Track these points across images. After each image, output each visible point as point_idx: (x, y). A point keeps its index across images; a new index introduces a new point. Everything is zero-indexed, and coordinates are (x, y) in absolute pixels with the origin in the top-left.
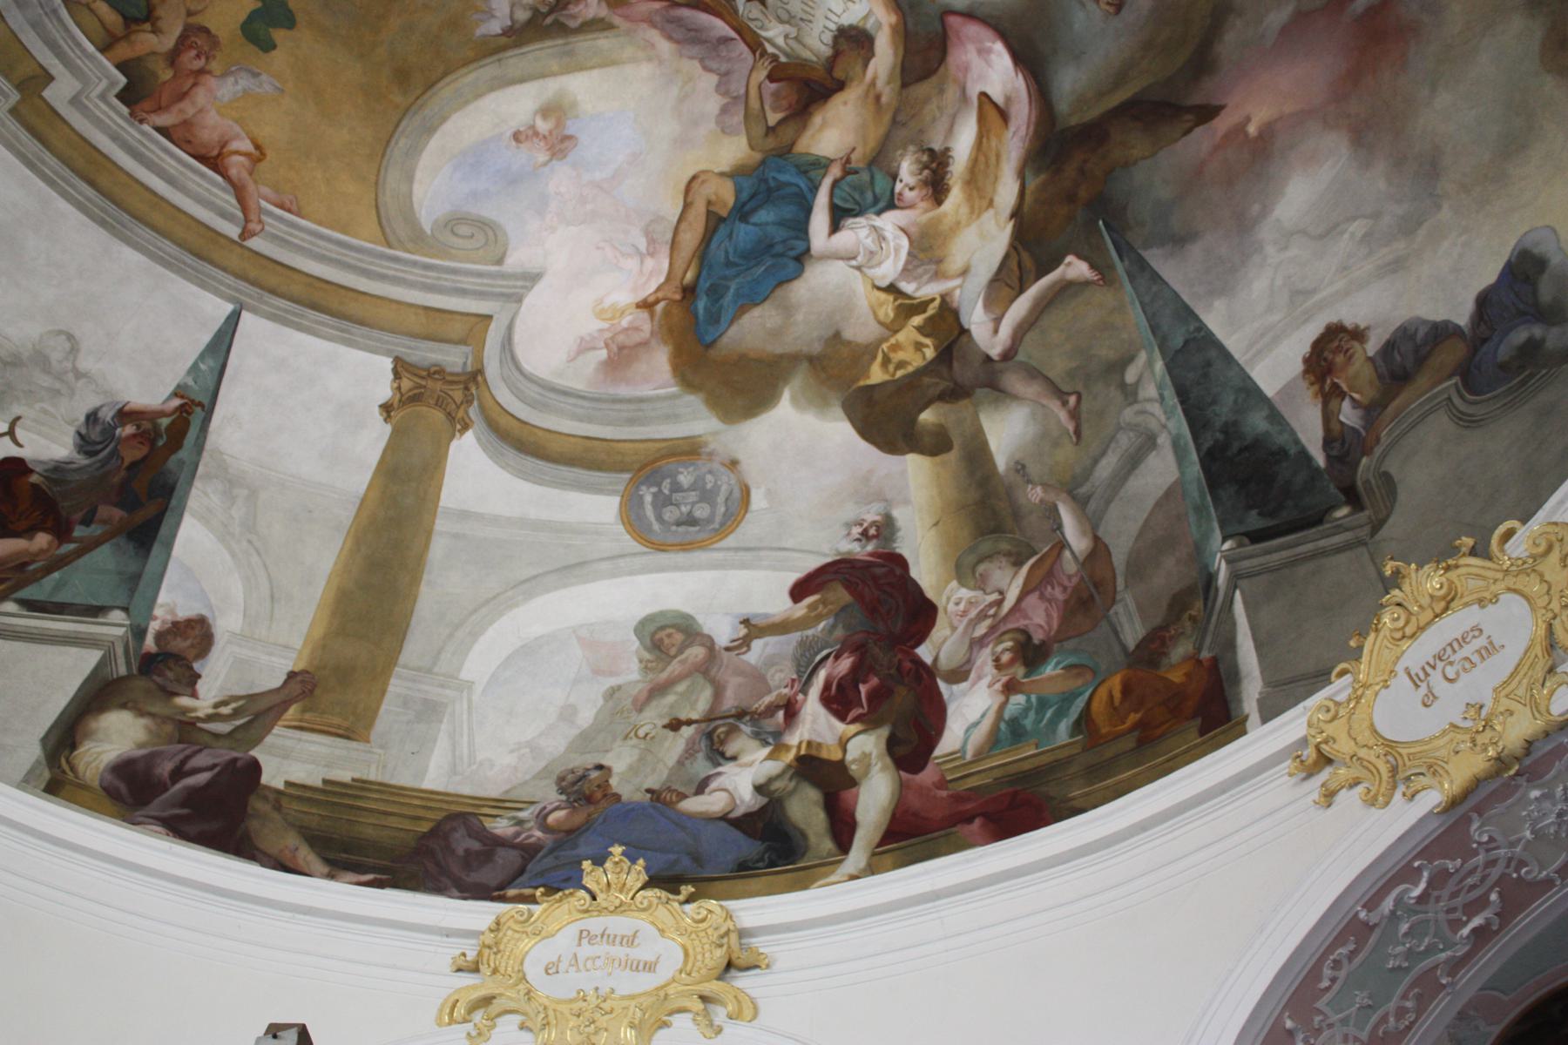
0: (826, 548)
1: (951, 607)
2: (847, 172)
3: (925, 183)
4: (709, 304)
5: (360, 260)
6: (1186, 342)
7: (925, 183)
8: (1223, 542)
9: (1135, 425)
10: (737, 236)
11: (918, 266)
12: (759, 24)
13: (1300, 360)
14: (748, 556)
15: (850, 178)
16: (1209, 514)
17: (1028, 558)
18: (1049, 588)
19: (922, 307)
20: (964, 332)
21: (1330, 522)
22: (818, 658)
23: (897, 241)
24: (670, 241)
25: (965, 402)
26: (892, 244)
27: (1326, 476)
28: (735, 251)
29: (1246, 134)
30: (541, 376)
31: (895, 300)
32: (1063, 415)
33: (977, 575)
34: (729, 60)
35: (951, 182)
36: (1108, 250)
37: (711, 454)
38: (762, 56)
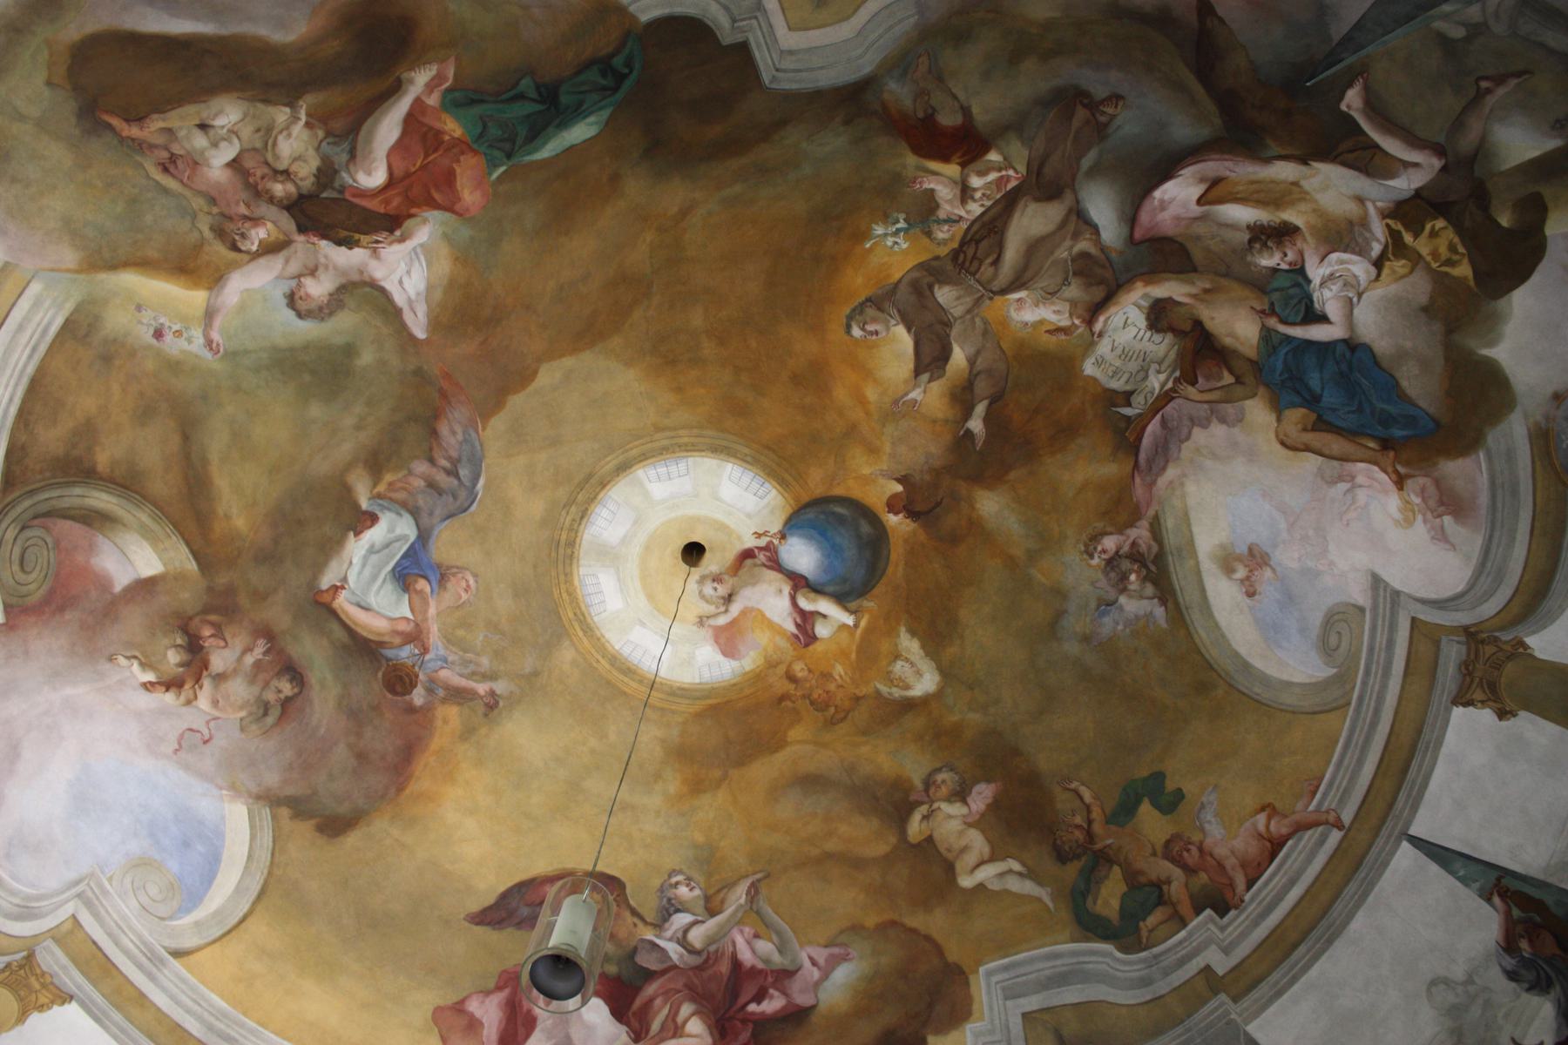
2: (1272, 312)
12: (1149, 395)
19: (1395, 236)
23: (1333, 262)
26: (1336, 268)
31: (1389, 260)
35: (1278, 221)
37: (1547, 418)
38: (1176, 391)
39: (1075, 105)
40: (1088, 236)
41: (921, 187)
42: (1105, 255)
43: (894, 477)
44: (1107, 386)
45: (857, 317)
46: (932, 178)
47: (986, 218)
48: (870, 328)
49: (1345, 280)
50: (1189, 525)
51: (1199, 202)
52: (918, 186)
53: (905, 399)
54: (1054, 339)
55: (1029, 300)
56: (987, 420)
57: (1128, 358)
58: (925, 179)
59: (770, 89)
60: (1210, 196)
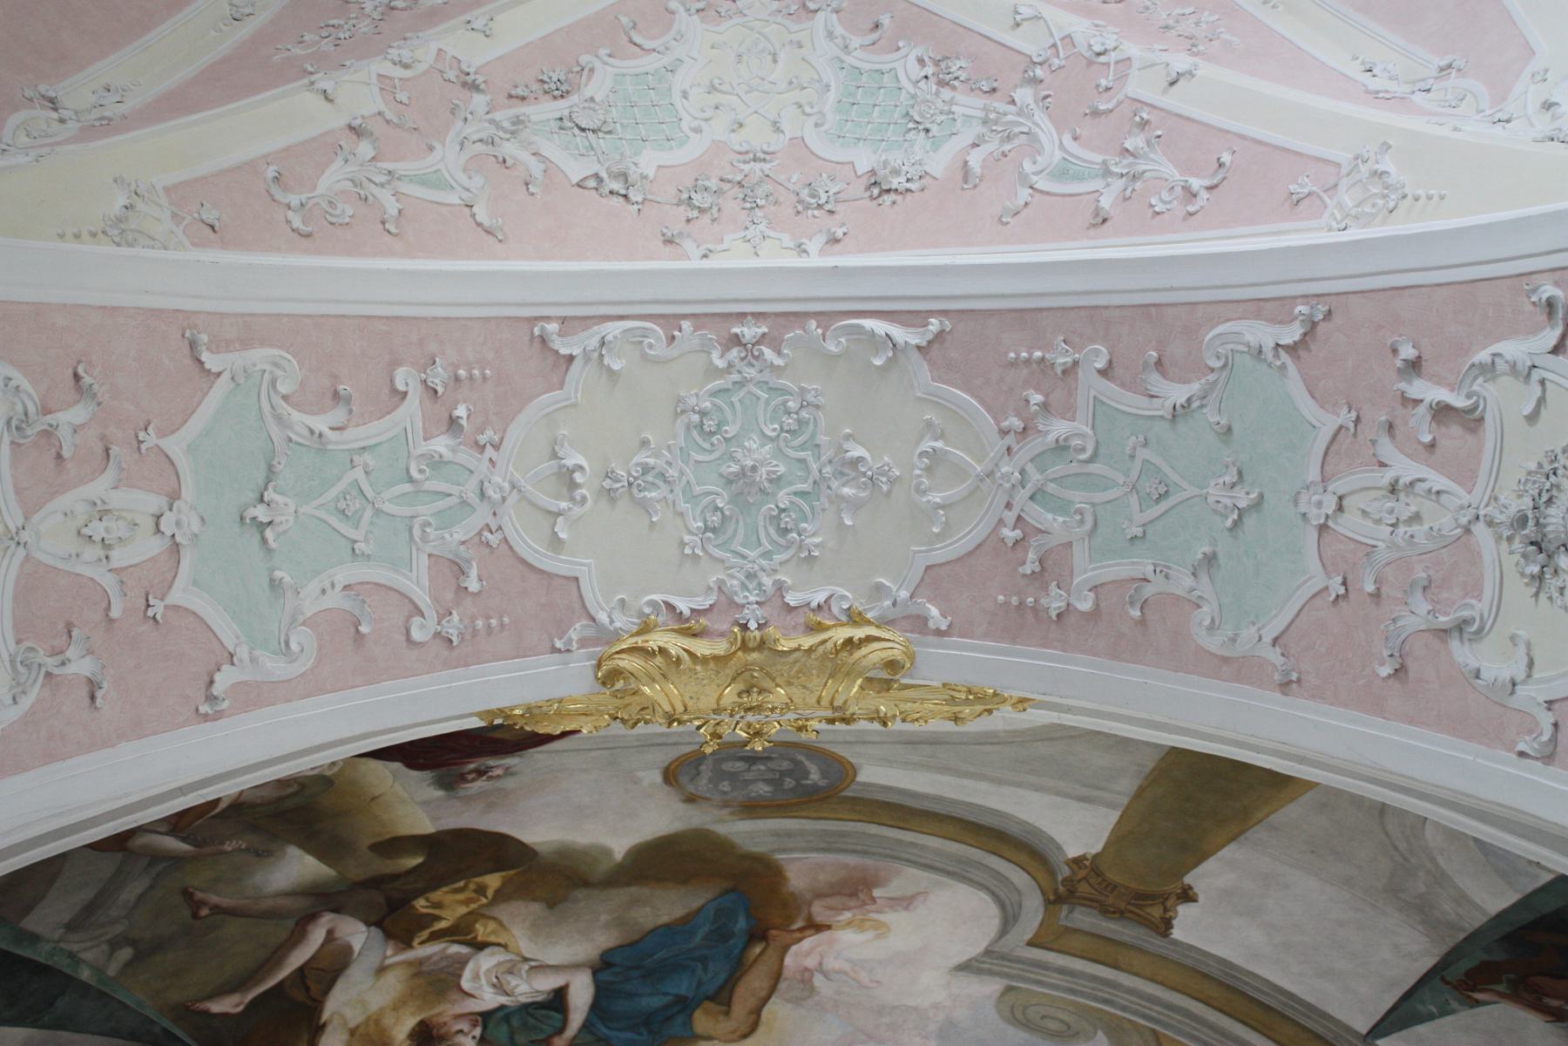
5: (1196, 1029)
11: (447, 967)
23: (477, 985)
24: (781, 980)
26: (483, 981)
30: (965, 886)
31: (476, 938)
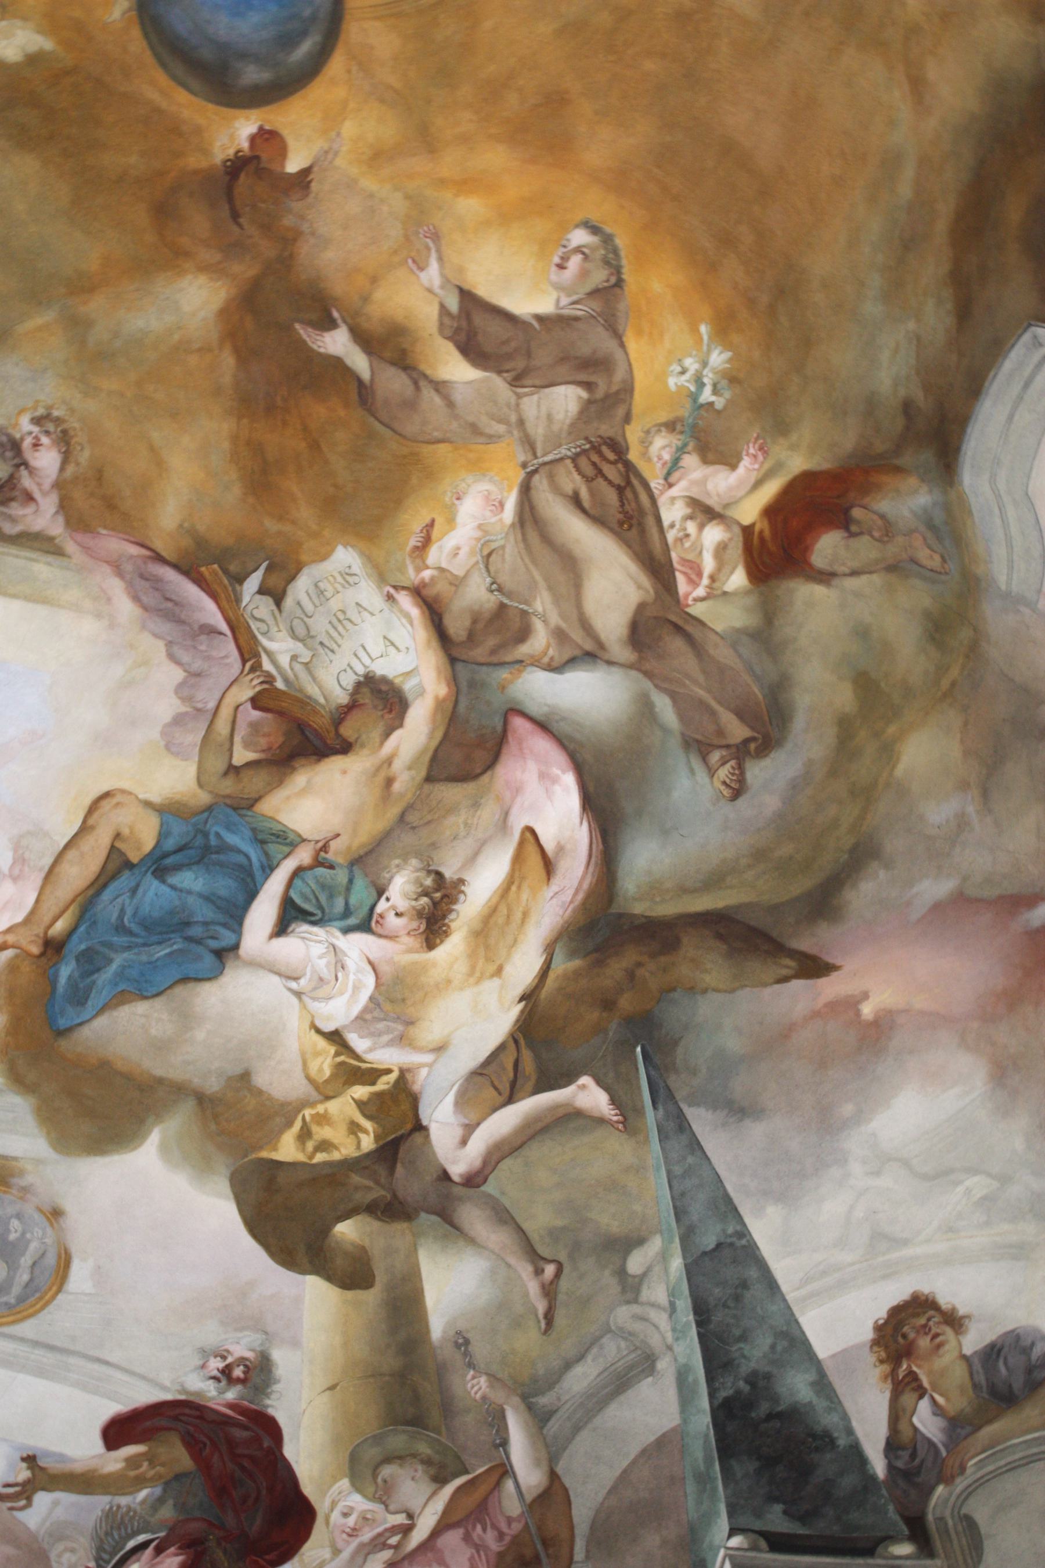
0: (166, 1378)
1: (335, 1516)
2: (318, 862)
3: (420, 914)
4: (76, 974)
6: (719, 1246)
7: (420, 914)
8: (730, 1536)
9: (630, 1334)
10: (144, 895)
12: (264, 628)
13: (870, 1324)
14: (48, 1358)
15: (320, 871)
16: (714, 1489)
17: (456, 1475)
18: (479, 1528)
19: (371, 1075)
20: (419, 1127)
21: (885, 1558)
22: (131, 1544)
23: (360, 976)
24: (47, 869)
25: (400, 1226)
26: (352, 977)
27: (884, 1492)
28: (135, 914)
29: (858, 1013)
31: (337, 1054)
32: (533, 1287)
33: (379, 1480)
34: (208, 658)
35: (453, 925)
36: (639, 1088)
37: (25, 1190)
38: (253, 670)
39: (752, 728)
40: (551, 652)
41: (748, 455)
42: (508, 663)
43: (315, 169)
44: (305, 571)
45: (603, 252)
46: (754, 477)
47: (650, 521)
48: (575, 261)
49: (328, 983)
50: (27, 598)
51: (531, 830)
52: (752, 451)
53: (434, 255)
54: (417, 526)
55: (493, 520)
56: (337, 364)
57: (335, 621)
58: (756, 466)
59: (1025, 330)
60: (531, 850)
